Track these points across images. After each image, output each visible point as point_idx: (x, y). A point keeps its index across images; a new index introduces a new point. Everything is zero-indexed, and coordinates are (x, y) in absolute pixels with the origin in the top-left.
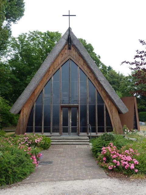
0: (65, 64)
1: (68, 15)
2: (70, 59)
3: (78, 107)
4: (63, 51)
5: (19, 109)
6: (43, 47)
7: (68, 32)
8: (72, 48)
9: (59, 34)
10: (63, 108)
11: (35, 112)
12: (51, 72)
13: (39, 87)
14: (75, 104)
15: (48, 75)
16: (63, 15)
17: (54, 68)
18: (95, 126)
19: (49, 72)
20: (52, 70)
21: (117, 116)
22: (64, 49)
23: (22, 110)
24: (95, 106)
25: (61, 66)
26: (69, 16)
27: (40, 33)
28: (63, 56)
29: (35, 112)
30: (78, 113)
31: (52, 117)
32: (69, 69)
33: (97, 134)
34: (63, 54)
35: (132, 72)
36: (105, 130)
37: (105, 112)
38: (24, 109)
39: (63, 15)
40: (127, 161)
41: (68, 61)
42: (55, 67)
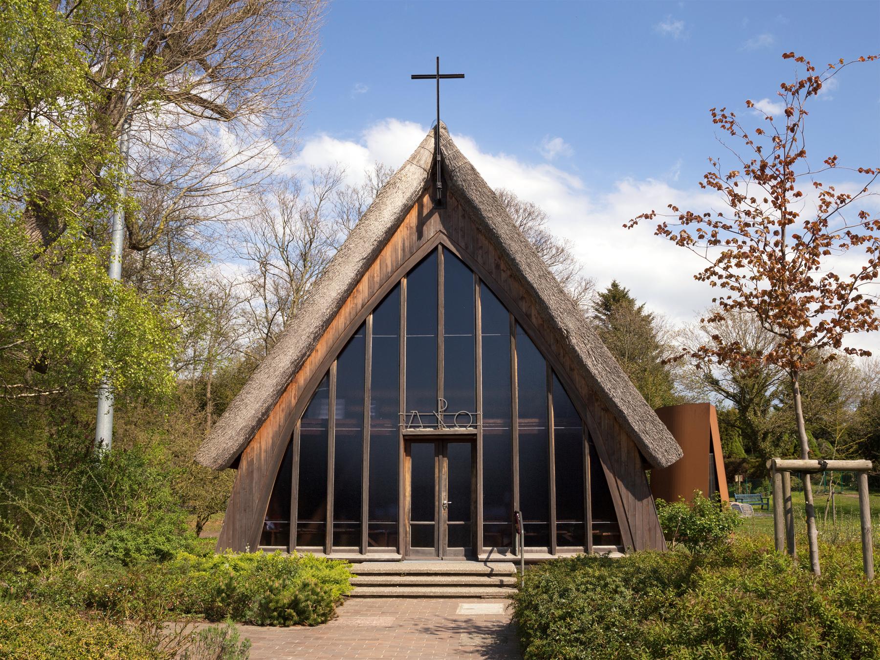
3: (476, 440)
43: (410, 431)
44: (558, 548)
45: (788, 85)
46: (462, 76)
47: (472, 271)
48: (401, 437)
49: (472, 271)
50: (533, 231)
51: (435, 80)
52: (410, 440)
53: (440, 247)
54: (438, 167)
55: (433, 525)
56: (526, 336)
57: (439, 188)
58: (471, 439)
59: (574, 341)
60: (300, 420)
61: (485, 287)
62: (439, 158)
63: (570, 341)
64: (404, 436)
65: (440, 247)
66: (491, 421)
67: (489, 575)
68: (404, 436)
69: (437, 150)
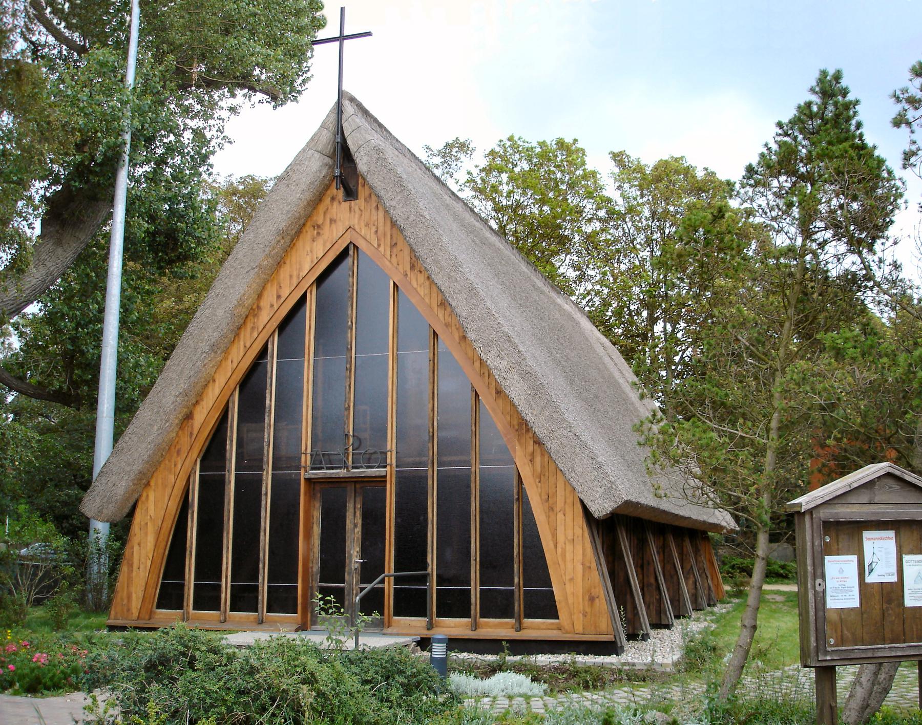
0: (313, 270)
4: (321, 208)
7: (334, 117)
9: (882, 159)
12: (264, 316)
13: (213, 389)
15: (253, 328)
17: (279, 297)
19: (255, 316)
20: (272, 306)
21: (578, 531)
22: (327, 200)
23: (140, 503)
26: (338, 43)
27: (688, 172)
28: (318, 234)
33: (475, 627)
34: (319, 226)
36: (518, 605)
38: (147, 496)
39: (368, 34)
40: (44, 483)
42: (285, 293)
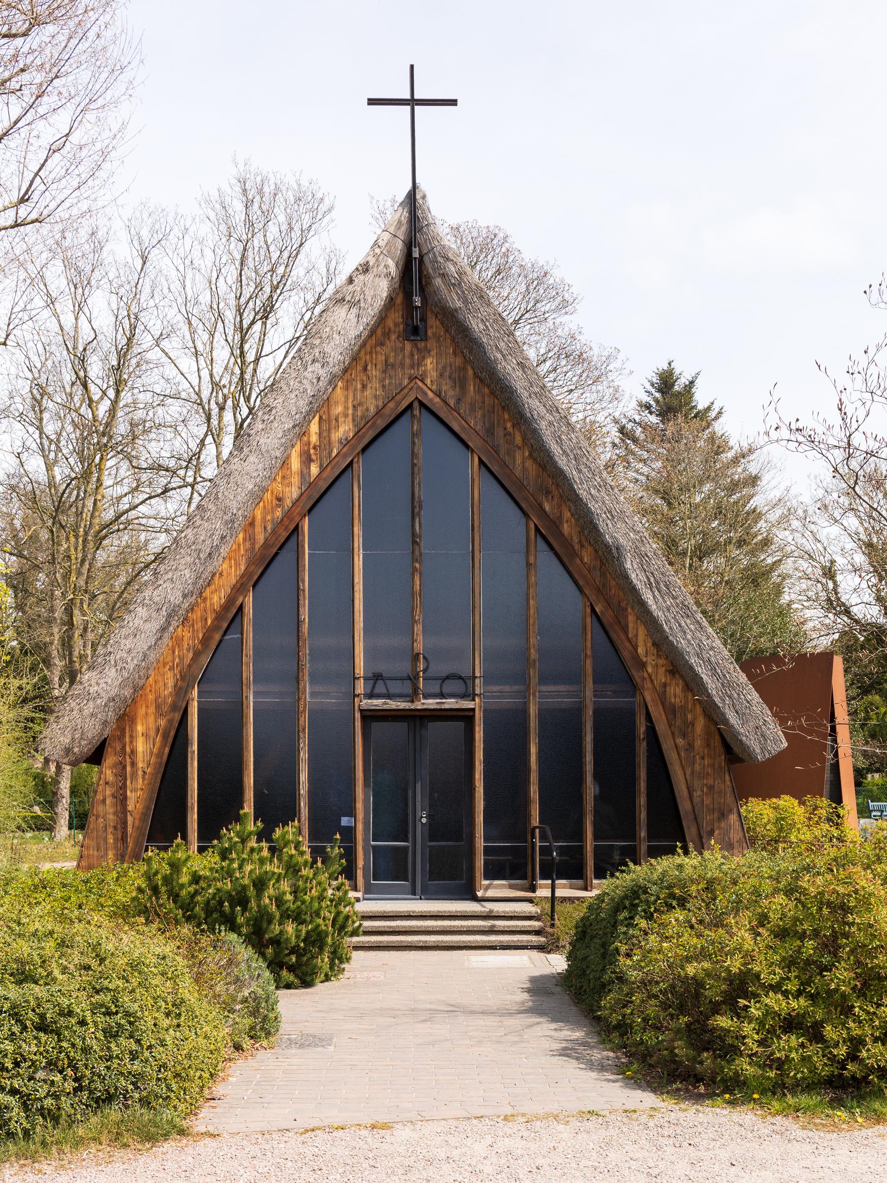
1: (408, 97)
2: (422, 405)
3: (473, 717)
5: (92, 730)
6: (716, 518)
8: (434, 326)
10: (376, 726)
11: (194, 747)
14: (451, 703)
16: (372, 102)
18: (579, 835)
24: (577, 712)
25: (364, 450)
29: (194, 747)
30: (529, 867)
31: (304, 789)
32: (42, 162)
35: (590, 432)
37: (642, 748)
39: (372, 102)
41: (406, 418)
43: (367, 703)
44: (595, 882)
45: (672, 364)
46: (453, 102)
47: (467, 446)
48: (358, 715)
49: (467, 446)
50: (159, 876)
51: (408, 108)
52: (369, 717)
53: (416, 404)
54: (563, 1053)
55: (405, 849)
56: (551, 554)
57: (417, 307)
58: (467, 717)
59: (628, 565)
60: (196, 686)
61: (488, 475)
62: (416, 254)
63: (622, 565)
64: (361, 711)
65: (416, 404)
66: (495, 688)
67: (492, 931)
68: (361, 711)
69: (410, 244)
